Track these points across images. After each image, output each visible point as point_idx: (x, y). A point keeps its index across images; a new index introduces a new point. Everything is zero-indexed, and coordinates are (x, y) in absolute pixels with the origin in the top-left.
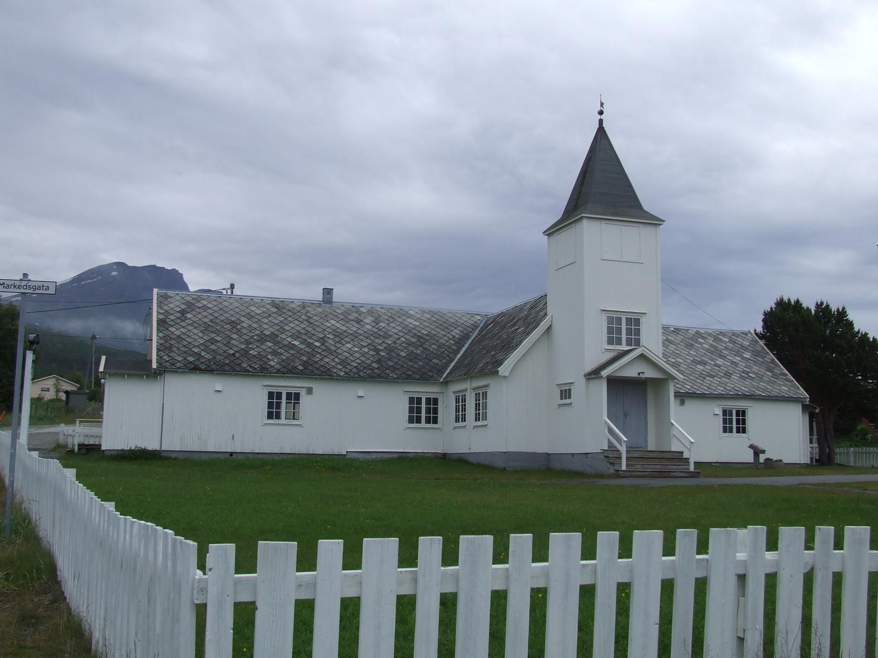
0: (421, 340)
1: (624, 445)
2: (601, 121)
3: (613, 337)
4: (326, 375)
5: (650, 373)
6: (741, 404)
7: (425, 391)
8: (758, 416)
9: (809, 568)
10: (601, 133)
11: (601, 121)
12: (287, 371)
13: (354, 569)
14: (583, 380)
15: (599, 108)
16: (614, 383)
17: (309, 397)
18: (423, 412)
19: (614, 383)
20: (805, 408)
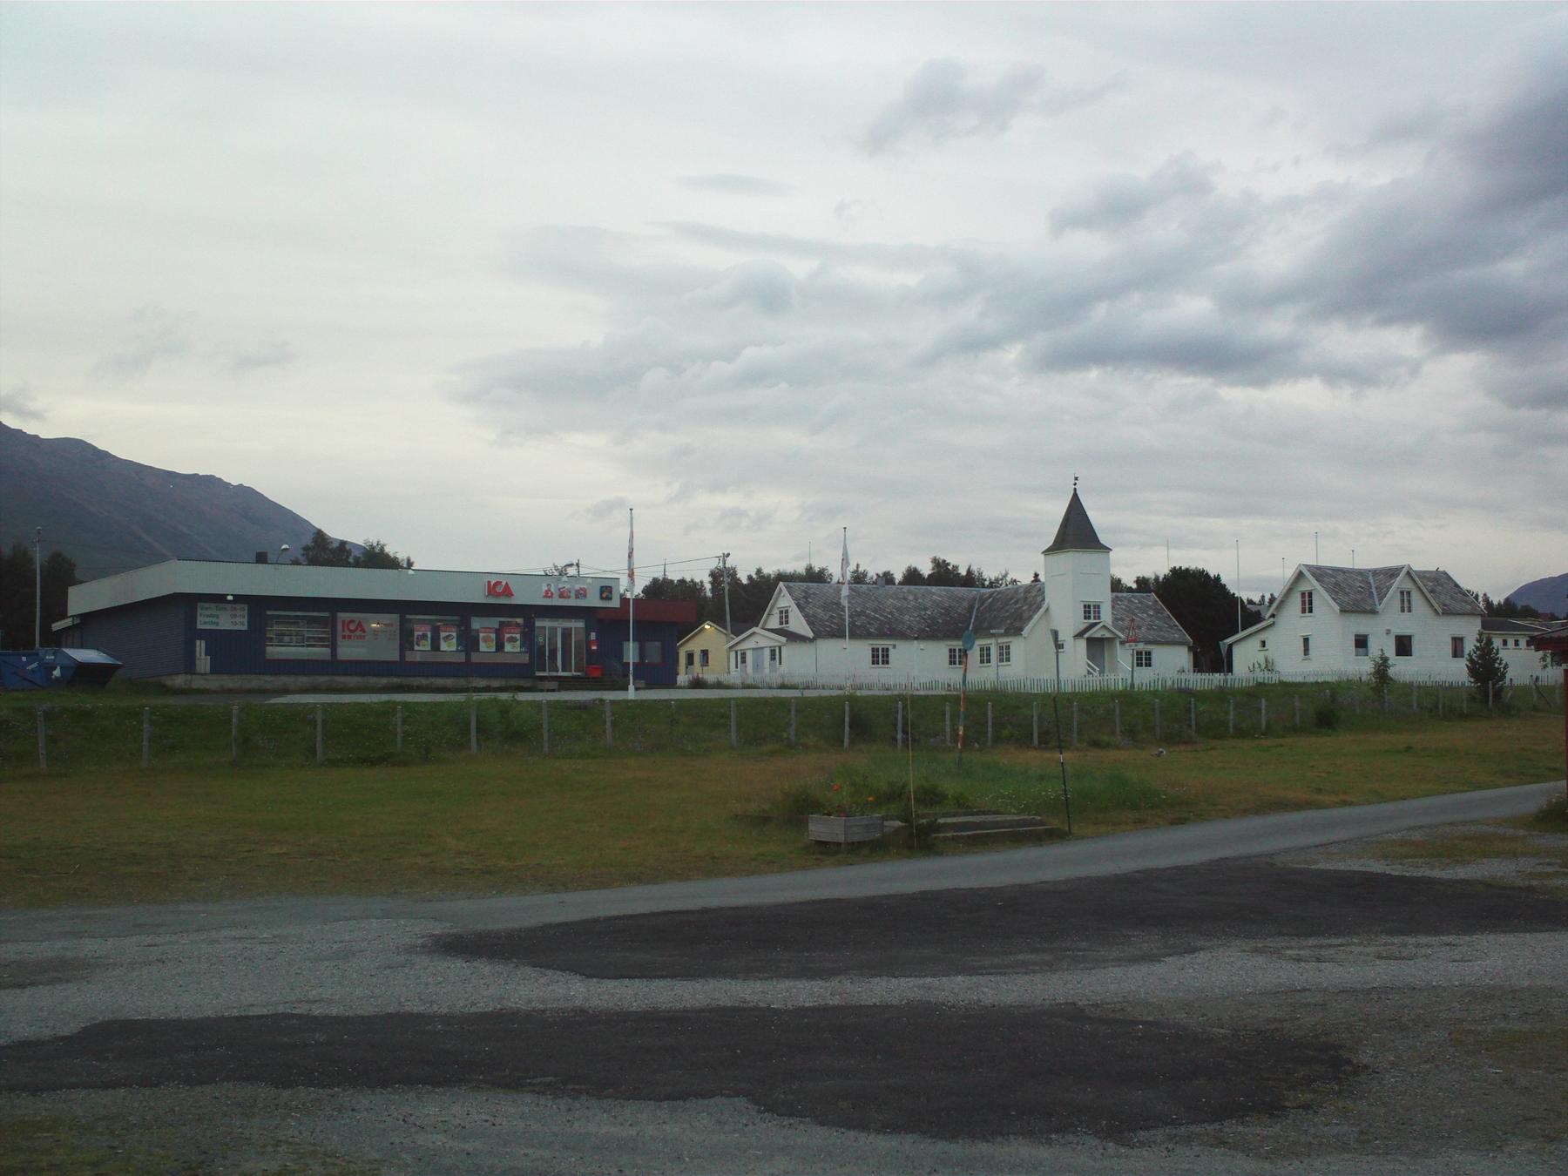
0: (948, 610)
3: (1087, 616)
4: (902, 636)
5: (1108, 635)
6: (1148, 648)
8: (1160, 654)
9: (1103, 538)
10: (1075, 496)
12: (881, 635)
16: (1090, 640)
18: (880, 657)
19: (1090, 640)
20: (1190, 649)
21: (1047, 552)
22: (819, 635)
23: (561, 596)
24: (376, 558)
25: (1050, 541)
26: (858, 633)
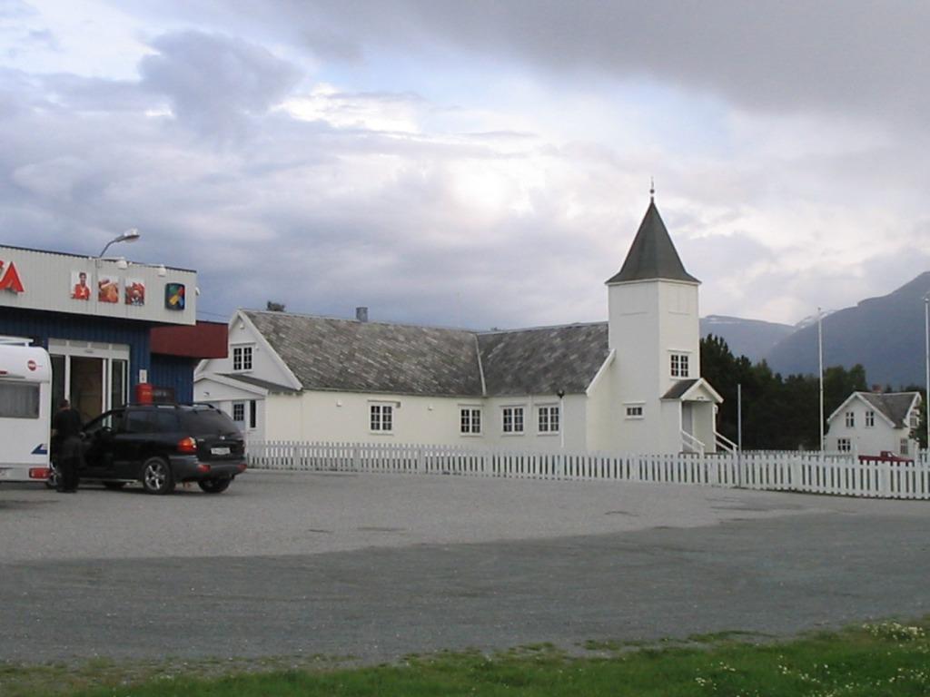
1: (702, 449)
2: (652, 199)
7: (471, 404)
10: (652, 207)
11: (652, 199)
12: (384, 389)
13: (840, 405)
14: (659, 402)
15: (650, 188)
17: (398, 410)
18: (381, 419)
21: (613, 281)
22: (307, 386)
23: (103, 297)
24: (23, 378)
25: (617, 268)
26: (442, 389)
